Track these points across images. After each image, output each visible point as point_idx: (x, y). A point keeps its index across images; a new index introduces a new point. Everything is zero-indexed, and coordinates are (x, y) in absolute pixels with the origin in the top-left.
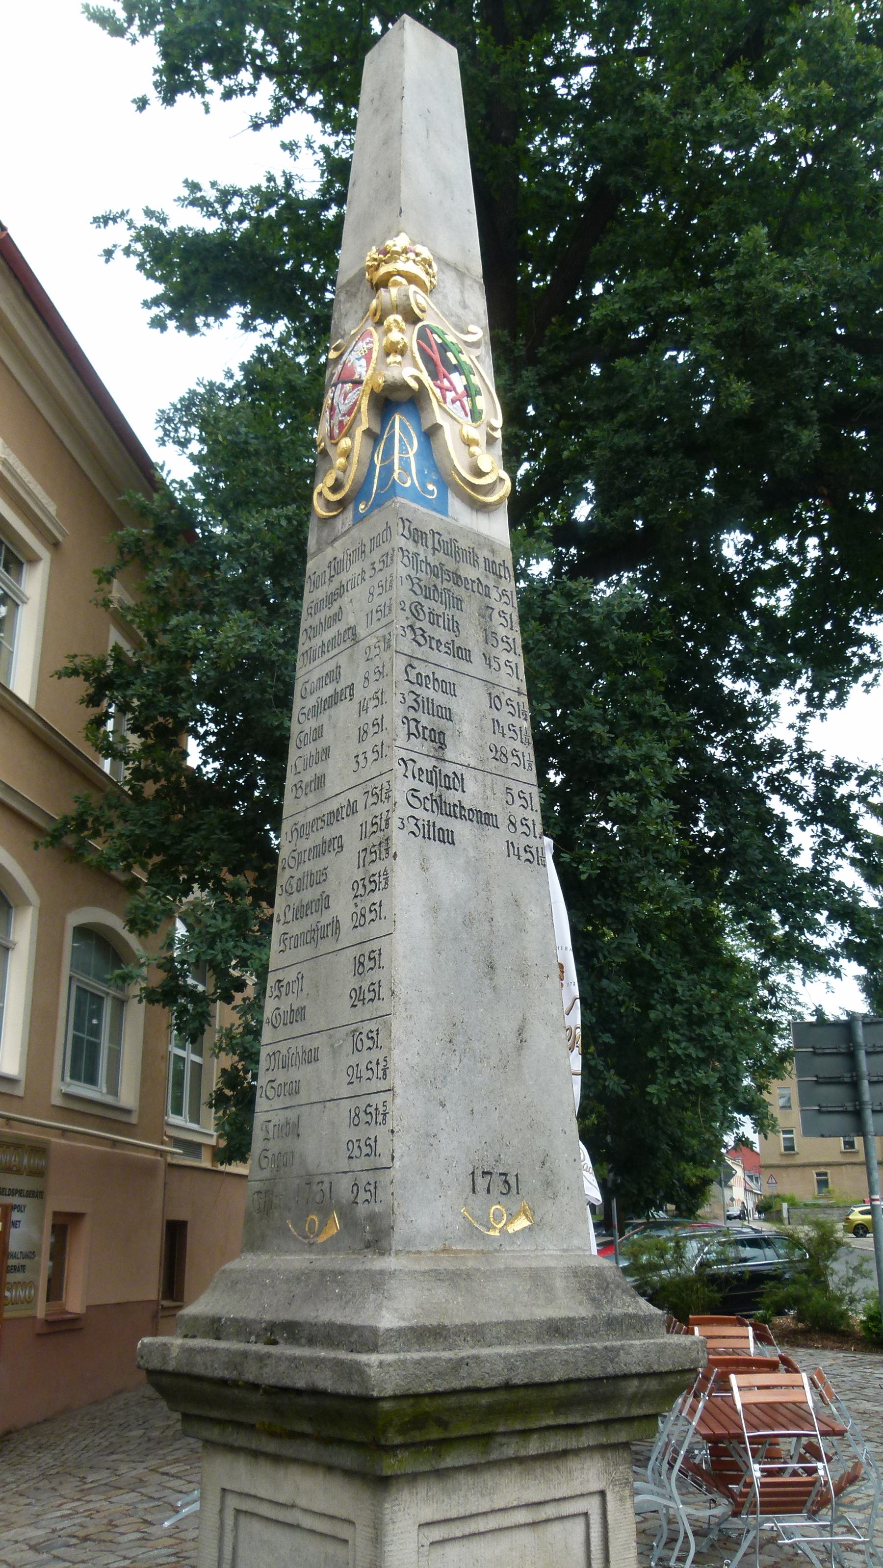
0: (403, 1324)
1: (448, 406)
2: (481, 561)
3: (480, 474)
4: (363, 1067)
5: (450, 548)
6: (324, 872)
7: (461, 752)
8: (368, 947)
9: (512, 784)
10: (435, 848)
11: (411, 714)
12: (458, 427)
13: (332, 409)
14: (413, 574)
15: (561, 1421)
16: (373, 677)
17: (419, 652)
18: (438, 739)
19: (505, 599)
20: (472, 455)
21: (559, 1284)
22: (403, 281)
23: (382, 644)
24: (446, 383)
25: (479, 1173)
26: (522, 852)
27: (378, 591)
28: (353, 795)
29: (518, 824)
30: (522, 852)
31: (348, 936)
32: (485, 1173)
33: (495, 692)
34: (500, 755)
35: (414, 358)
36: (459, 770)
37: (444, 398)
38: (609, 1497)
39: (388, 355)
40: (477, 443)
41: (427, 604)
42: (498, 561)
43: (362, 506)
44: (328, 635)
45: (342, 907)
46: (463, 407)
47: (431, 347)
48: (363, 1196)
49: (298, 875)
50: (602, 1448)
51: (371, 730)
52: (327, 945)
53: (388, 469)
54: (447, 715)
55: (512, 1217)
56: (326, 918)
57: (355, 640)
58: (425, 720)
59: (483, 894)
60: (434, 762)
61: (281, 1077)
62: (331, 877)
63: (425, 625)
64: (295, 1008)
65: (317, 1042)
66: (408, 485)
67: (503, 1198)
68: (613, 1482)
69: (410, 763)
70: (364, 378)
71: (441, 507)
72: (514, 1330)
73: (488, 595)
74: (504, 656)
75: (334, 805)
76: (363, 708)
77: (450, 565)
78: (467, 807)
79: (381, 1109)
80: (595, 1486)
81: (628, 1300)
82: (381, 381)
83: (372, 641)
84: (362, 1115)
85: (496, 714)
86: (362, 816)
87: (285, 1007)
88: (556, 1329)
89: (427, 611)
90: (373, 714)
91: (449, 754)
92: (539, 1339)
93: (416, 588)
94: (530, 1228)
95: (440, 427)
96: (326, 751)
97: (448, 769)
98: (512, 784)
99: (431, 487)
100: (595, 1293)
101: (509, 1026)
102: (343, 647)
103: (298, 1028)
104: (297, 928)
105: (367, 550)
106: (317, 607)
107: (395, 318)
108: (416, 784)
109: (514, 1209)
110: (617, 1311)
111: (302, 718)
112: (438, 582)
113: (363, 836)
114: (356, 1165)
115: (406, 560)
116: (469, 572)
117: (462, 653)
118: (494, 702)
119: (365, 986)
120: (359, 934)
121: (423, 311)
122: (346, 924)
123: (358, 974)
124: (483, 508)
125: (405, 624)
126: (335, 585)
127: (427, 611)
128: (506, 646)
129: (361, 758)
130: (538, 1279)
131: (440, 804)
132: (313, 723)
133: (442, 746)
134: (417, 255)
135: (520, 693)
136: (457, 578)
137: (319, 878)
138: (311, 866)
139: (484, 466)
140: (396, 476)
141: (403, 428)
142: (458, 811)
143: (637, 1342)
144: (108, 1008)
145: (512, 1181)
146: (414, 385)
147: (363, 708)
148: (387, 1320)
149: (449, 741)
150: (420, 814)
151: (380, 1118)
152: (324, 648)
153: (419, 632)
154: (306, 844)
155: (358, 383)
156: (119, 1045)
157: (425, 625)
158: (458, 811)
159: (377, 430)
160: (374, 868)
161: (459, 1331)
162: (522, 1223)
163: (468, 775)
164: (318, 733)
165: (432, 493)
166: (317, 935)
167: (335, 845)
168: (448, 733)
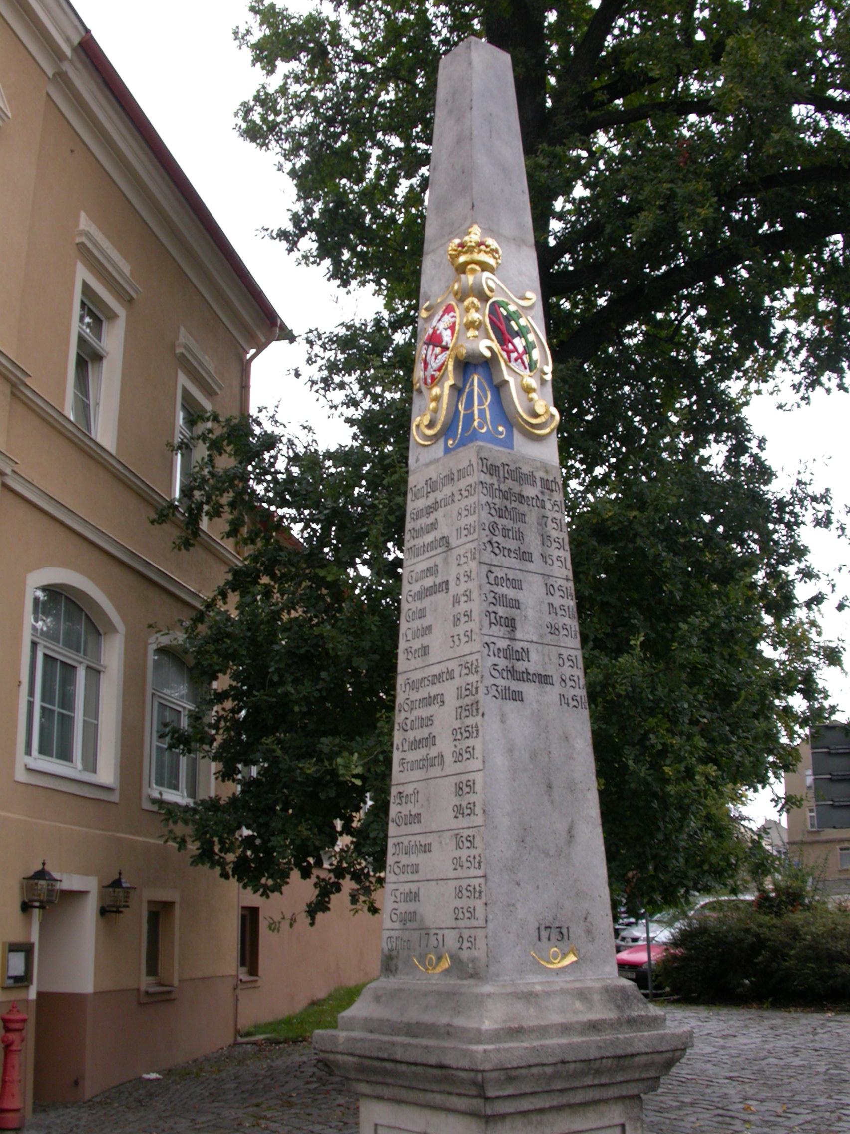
0: (496, 1026)
1: (513, 365)
2: (538, 481)
3: (536, 415)
4: (464, 859)
5: (518, 476)
6: (431, 718)
7: (526, 633)
8: (464, 778)
9: (563, 651)
10: (510, 705)
11: (492, 608)
12: (519, 379)
13: (426, 364)
14: (490, 500)
15: (596, 1082)
16: (463, 579)
17: (496, 560)
18: (511, 624)
19: (556, 508)
20: (531, 400)
21: (596, 997)
22: (478, 268)
23: (469, 555)
24: (511, 347)
25: (542, 928)
26: (570, 701)
27: (465, 513)
28: (452, 665)
29: (567, 681)
30: (570, 701)
31: (450, 767)
32: (546, 928)
33: (551, 581)
34: (554, 630)
35: (487, 330)
36: (525, 645)
37: (509, 357)
38: (627, 1127)
39: (468, 329)
40: (534, 390)
41: (501, 522)
42: (551, 478)
43: (451, 442)
44: (428, 538)
45: (445, 746)
46: (523, 363)
47: (499, 320)
48: (466, 945)
49: (412, 717)
50: (622, 1098)
51: (464, 619)
52: (435, 771)
53: (469, 418)
54: (516, 604)
55: (564, 956)
56: (434, 752)
57: (449, 547)
58: (501, 611)
59: (543, 735)
60: (508, 642)
61: (404, 860)
62: (436, 723)
63: (499, 538)
64: (413, 813)
65: (430, 838)
66: (484, 431)
67: (558, 943)
68: (630, 1118)
69: (492, 646)
70: (451, 346)
71: (508, 443)
72: (566, 1029)
73: (544, 507)
74: (556, 553)
75: (436, 670)
76: (456, 601)
77: (517, 489)
78: (531, 672)
79: (478, 889)
80: (618, 1120)
81: (641, 1006)
82: (465, 351)
83: (462, 551)
84: (464, 892)
85: (551, 599)
86: (458, 682)
87: (405, 812)
88: (594, 1026)
89: (500, 527)
90: (464, 607)
91: (519, 635)
92: (582, 1033)
93: (493, 512)
94: (576, 962)
95: (507, 382)
96: (430, 628)
97: (518, 646)
98: (563, 651)
99: (501, 429)
100: (619, 1002)
101: (562, 826)
102: (440, 550)
103: (415, 828)
104: (412, 756)
105: (456, 478)
106: (418, 515)
107: (473, 311)
108: (496, 660)
109: (566, 950)
110: (635, 1014)
111: (410, 599)
112: (507, 503)
113: (460, 697)
114: (461, 924)
115: (485, 491)
116: (530, 491)
117: (525, 556)
118: (549, 590)
119: (464, 804)
120: (459, 767)
121: (491, 290)
122: (449, 758)
123: (457, 794)
124: (540, 439)
125: (486, 540)
126: (430, 501)
127: (500, 527)
128: (557, 545)
129: (456, 638)
130: (582, 995)
131: (513, 674)
132: (418, 605)
133: (514, 629)
134: (487, 246)
135: (567, 580)
136: (521, 498)
137: (428, 721)
138: (423, 712)
139: (540, 409)
140: (476, 424)
141: (480, 386)
142: (524, 677)
143: (646, 1033)
144: (81, 674)
145: (564, 931)
146: (488, 354)
147: (456, 601)
148: (487, 1025)
149: (518, 625)
150: (501, 682)
151: (477, 895)
152: (425, 548)
153: (495, 545)
154: (416, 696)
155: (445, 349)
156: (97, 718)
157: (499, 538)
158: (524, 677)
159: (460, 385)
160: (471, 721)
161: (532, 1030)
162: (571, 958)
163: (532, 648)
164: (422, 614)
165: (501, 433)
166: (428, 763)
167: (437, 700)
168: (517, 619)
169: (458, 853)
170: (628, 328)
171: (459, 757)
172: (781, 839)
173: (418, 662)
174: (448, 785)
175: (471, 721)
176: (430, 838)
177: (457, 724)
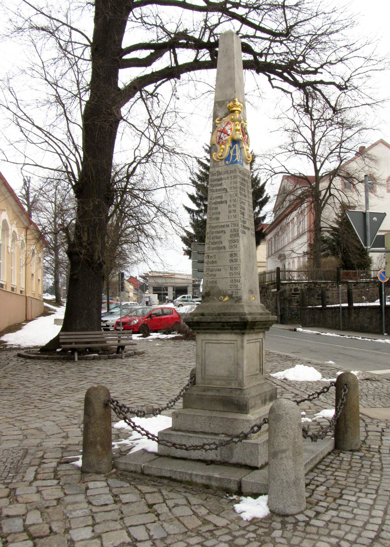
8: (233, 253)
52: (223, 250)
86: (230, 228)
103: (215, 265)
120: (231, 250)
147: (229, 206)
155: (229, 135)
169: (231, 271)
170: (112, 174)
171: (231, 247)
172: (60, 470)
173: (215, 221)
174: (227, 255)
175: (235, 238)
176: (220, 268)
177: (231, 239)
